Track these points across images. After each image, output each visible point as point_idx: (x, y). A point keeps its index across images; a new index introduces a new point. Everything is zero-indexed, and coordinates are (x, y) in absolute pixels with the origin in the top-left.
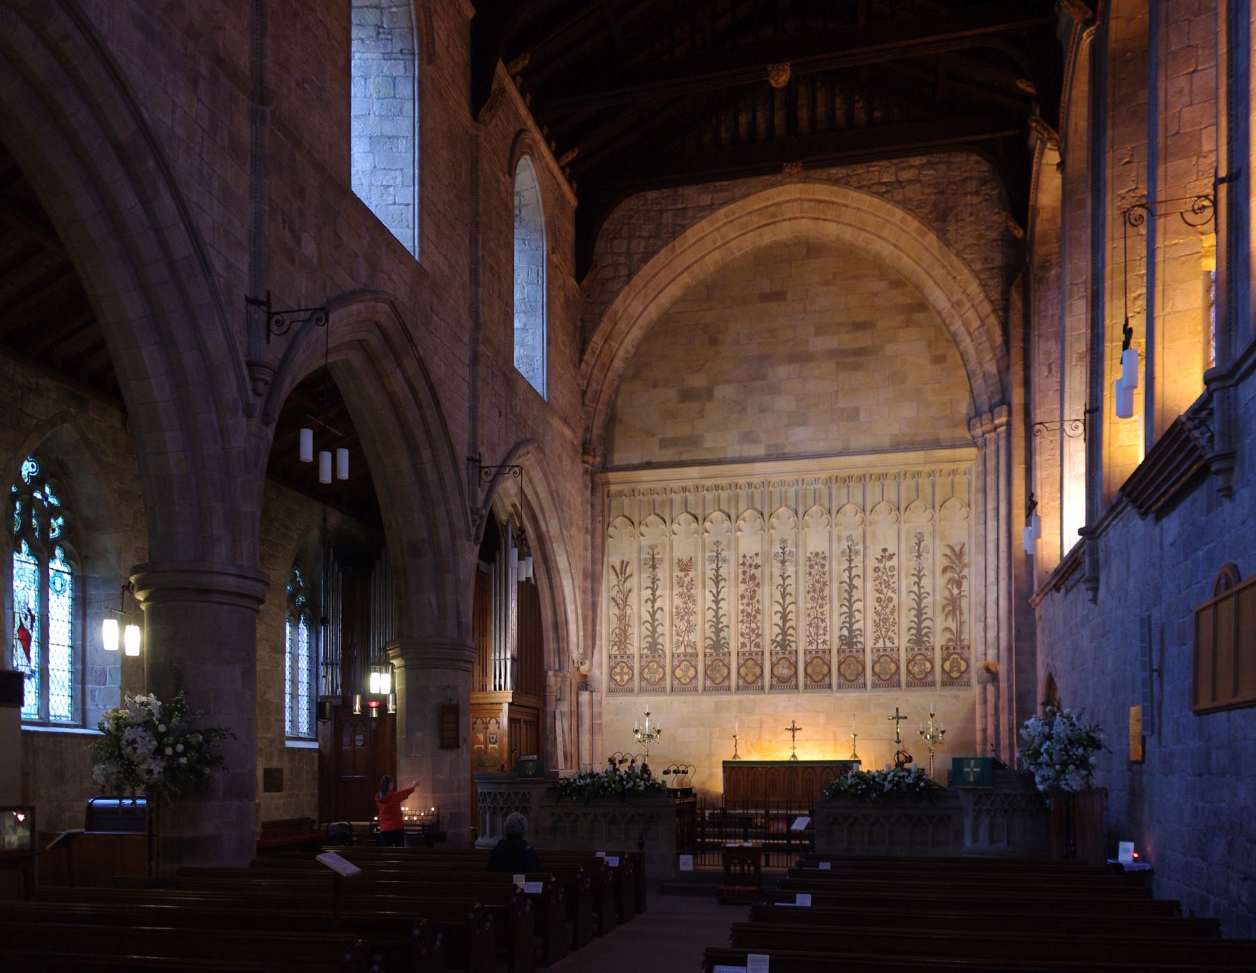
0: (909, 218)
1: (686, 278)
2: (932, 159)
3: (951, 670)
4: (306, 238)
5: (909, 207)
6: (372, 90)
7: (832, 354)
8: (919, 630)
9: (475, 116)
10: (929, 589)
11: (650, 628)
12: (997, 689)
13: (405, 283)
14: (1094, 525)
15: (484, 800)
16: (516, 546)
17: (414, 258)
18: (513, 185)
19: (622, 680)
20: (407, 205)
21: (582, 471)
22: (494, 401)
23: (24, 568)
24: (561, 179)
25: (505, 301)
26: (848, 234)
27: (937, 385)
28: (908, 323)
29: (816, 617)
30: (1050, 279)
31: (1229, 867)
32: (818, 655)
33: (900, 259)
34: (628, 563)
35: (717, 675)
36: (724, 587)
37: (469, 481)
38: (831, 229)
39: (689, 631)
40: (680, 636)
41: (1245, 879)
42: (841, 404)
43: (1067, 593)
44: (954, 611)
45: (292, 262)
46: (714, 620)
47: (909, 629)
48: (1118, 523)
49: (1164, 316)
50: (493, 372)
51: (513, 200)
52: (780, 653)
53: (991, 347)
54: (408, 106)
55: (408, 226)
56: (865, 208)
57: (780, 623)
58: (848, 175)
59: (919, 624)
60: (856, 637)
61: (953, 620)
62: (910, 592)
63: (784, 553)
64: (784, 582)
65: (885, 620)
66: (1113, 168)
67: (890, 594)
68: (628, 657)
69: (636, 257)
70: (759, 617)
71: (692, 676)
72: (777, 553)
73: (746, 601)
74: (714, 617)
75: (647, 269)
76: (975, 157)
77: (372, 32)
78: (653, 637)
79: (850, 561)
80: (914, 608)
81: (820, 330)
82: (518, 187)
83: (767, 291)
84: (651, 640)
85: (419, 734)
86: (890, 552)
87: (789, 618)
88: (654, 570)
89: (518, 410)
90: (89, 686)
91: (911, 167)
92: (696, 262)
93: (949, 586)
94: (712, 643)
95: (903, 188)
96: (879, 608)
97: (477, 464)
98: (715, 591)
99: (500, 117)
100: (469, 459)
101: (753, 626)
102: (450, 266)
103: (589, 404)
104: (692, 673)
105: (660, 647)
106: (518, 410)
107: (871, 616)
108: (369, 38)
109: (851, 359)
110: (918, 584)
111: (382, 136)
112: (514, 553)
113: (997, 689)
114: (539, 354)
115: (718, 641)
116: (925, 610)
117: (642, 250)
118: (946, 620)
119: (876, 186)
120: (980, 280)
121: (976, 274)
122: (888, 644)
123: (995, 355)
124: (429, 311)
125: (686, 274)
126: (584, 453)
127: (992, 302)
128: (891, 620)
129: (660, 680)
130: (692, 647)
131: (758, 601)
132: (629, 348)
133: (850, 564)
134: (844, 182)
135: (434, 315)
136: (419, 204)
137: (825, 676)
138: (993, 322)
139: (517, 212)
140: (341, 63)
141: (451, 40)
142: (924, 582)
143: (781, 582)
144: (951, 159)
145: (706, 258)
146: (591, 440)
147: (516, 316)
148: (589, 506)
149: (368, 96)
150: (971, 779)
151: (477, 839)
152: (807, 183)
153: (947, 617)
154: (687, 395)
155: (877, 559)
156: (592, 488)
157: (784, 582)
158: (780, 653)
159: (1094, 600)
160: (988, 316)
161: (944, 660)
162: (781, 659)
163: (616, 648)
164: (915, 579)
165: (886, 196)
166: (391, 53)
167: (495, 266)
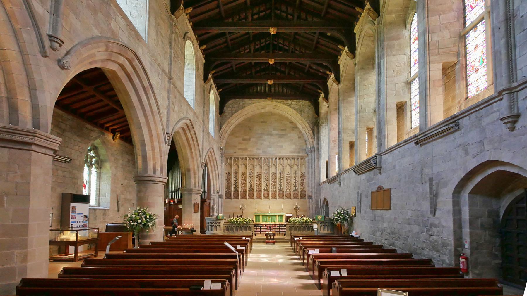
7: (277, 134)
8: (295, 188)
12: (312, 200)
15: (209, 224)
23: (86, 169)
24: (218, 94)
41: (386, 239)
45: (174, 111)
54: (193, 80)
78: (236, 188)
81: (274, 130)
90: (100, 198)
107: (285, 185)
109: (281, 136)
122: (289, 191)
134: (281, 103)
138: (311, 132)
159: (340, 186)
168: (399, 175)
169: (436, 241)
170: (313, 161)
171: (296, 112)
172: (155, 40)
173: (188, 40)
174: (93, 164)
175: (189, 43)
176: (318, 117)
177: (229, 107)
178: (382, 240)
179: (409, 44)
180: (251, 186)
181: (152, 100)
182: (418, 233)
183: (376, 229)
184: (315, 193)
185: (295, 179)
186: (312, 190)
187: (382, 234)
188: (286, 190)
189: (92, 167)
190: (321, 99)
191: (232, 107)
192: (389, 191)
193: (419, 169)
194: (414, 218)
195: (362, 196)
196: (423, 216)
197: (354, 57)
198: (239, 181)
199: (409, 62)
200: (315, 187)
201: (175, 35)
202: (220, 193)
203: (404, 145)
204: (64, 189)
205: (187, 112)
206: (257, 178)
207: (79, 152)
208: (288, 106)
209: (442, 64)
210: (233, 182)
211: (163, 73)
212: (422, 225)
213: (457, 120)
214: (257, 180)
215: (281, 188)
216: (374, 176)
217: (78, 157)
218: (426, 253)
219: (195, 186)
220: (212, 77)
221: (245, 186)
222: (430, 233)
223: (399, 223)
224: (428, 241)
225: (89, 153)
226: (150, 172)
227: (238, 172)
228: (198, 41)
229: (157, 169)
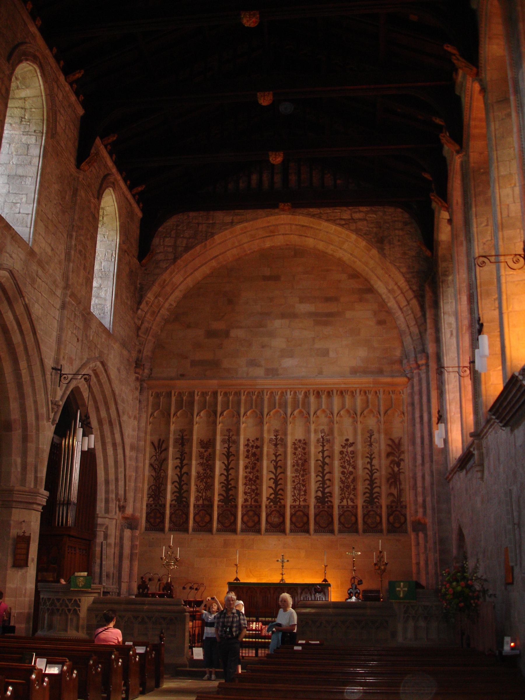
0: (360, 240)
1: (214, 263)
2: (373, 208)
5: (359, 233)
6: (13, 149)
7: (311, 314)
8: (371, 494)
9: (78, 165)
10: (377, 467)
11: (178, 486)
12: (426, 536)
13: (21, 259)
14: (479, 431)
16: (81, 427)
17: (28, 245)
18: (100, 204)
20: (28, 214)
21: (134, 378)
22: (74, 332)
24: (132, 201)
25: (88, 271)
26: (321, 246)
27: (379, 338)
28: (361, 300)
29: (299, 483)
30: (449, 281)
32: (300, 509)
33: (355, 262)
34: (164, 441)
35: (226, 521)
36: (233, 460)
37: (51, 382)
38: (310, 242)
39: (206, 490)
40: (200, 493)
42: (317, 346)
43: (467, 473)
46: (225, 482)
47: (365, 493)
48: (492, 431)
49: (508, 313)
50: (75, 314)
51: (98, 213)
52: (273, 507)
53: (415, 317)
54: (35, 161)
55: (27, 227)
56: (332, 232)
57: (273, 486)
58: (321, 213)
59: (372, 489)
61: (395, 488)
62: (365, 468)
63: (276, 439)
64: (276, 458)
65: (348, 487)
66: (477, 228)
67: (351, 469)
68: (161, 506)
69: (180, 249)
70: (258, 481)
71: (207, 521)
72: (272, 439)
73: (248, 470)
74: (225, 480)
75: (187, 256)
76: (400, 210)
77: (18, 120)
79: (323, 446)
80: (367, 479)
82: (102, 205)
84: (178, 495)
86: (351, 441)
87: (279, 483)
88: (182, 446)
89: (91, 338)
91: (360, 212)
92: (220, 254)
93: (392, 466)
94: (223, 498)
95: (356, 223)
96: (344, 479)
97: (59, 372)
98: (226, 462)
99: (95, 167)
100: (53, 369)
101: (253, 487)
102: (52, 250)
103: (142, 335)
105: (184, 499)
106: (91, 338)
108: (15, 123)
110: (370, 463)
111: (16, 175)
112: (80, 431)
113: (426, 536)
114: (108, 304)
116: (376, 481)
117: (184, 245)
119: (338, 220)
120: (406, 278)
121: (403, 274)
122: (350, 503)
123: (417, 322)
124: (36, 276)
125: (213, 261)
126: (136, 367)
127: (414, 291)
128: (352, 487)
130: (208, 501)
131: (258, 471)
132: (173, 303)
133: (323, 448)
135: (38, 278)
136: (36, 214)
139: (101, 218)
141: (67, 126)
142: (375, 462)
143: (275, 459)
144: (385, 210)
145: (228, 253)
146: (142, 358)
147: (95, 279)
148: (138, 402)
149: (10, 153)
150: (401, 595)
151: (37, 631)
152: (295, 215)
154: (211, 334)
155: (342, 445)
156: (141, 390)
157: (276, 458)
158: (273, 507)
160: (411, 299)
161: (389, 515)
162: (273, 511)
164: (369, 460)
165: (345, 226)
166: (28, 132)
167: (83, 251)
175: (31, 68)
186: (424, 501)
198: (190, 469)
208: (342, 225)
227: (190, 440)
228: (62, 63)
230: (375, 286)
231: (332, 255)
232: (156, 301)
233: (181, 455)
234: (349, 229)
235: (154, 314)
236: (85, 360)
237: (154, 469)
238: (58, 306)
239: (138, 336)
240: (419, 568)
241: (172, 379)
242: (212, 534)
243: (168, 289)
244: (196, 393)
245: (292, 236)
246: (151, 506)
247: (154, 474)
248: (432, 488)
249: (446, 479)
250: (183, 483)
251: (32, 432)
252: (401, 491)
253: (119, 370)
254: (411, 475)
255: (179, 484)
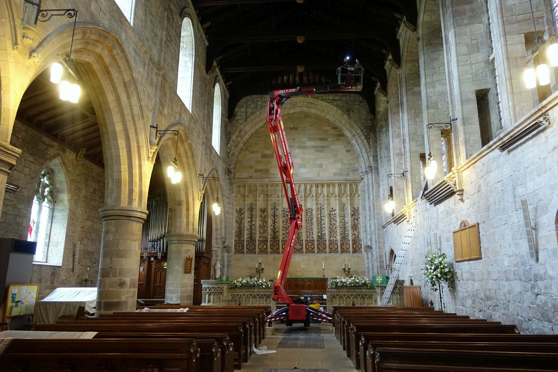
3: (356, 248)
4: (165, 108)
7: (313, 147)
12: (372, 254)
15: (206, 290)
19: (239, 249)
23: (35, 202)
24: (226, 89)
27: (348, 159)
28: (338, 140)
31: (474, 308)
38: (313, 111)
41: (480, 311)
42: (317, 162)
44: (356, 228)
45: (162, 115)
47: (341, 234)
59: (345, 232)
60: (323, 236)
67: (334, 222)
69: (249, 114)
73: (284, 223)
75: (252, 117)
78: (251, 234)
81: (309, 140)
83: (292, 127)
85: (176, 267)
86: (334, 209)
88: (252, 212)
90: (50, 248)
95: (336, 101)
98: (273, 220)
101: (287, 231)
102: (198, 115)
104: (265, 247)
115: (275, 236)
116: (347, 228)
117: (250, 112)
118: (353, 231)
120: (361, 129)
121: (360, 127)
122: (334, 239)
127: (365, 136)
128: (335, 231)
129: (253, 249)
137: (313, 249)
140: (177, 58)
153: (354, 230)
154: (264, 156)
161: (353, 245)
163: (237, 238)
168: (487, 201)
169: (546, 303)
170: (371, 188)
171: (340, 112)
172: (142, 20)
173: (187, 16)
174: (46, 197)
175: (187, 20)
176: (375, 118)
177: (242, 106)
178: (475, 313)
179: (486, 9)
180: (274, 231)
181: (134, 100)
182: (521, 292)
183: (465, 295)
184: (376, 241)
185: (344, 219)
186: (371, 238)
187: (474, 302)
188: (330, 237)
189: (44, 200)
190: (376, 92)
191: (247, 107)
192: (476, 227)
193: (510, 188)
194: (513, 269)
195: (442, 240)
196: (524, 264)
197: (415, 29)
198: (256, 223)
199: (489, 33)
200: (375, 232)
201: (169, 12)
202: (226, 244)
203: (488, 153)
204: (3, 232)
205: (180, 116)
206: (284, 218)
207: (29, 177)
208: (329, 103)
209: (523, 35)
210: (247, 225)
211: (151, 63)
212: (524, 280)
213: (546, 111)
214: (283, 222)
215: (321, 234)
216: (455, 205)
217: (28, 184)
218: (534, 327)
219: (188, 229)
220: (218, 65)
221: (265, 231)
222: (536, 291)
223: (495, 280)
224: (535, 306)
225: (42, 180)
226: (124, 203)
227: (255, 209)
228: (200, 18)
229: (134, 198)
230: (345, 133)
231: (324, 117)
232: (237, 140)
233: (251, 216)
234: (332, 104)
235: (236, 146)
236: (211, 170)
237: (238, 223)
238: (201, 144)
239: (228, 157)
240: (369, 270)
241: (246, 178)
242: (244, 254)
243: (243, 134)
244: (258, 185)
245: (304, 108)
246: (237, 241)
247: (238, 225)
248: (375, 232)
249: (383, 227)
250: (252, 229)
251: (191, 207)
252: (359, 233)
253: (222, 174)
254: (364, 225)
255: (251, 230)
